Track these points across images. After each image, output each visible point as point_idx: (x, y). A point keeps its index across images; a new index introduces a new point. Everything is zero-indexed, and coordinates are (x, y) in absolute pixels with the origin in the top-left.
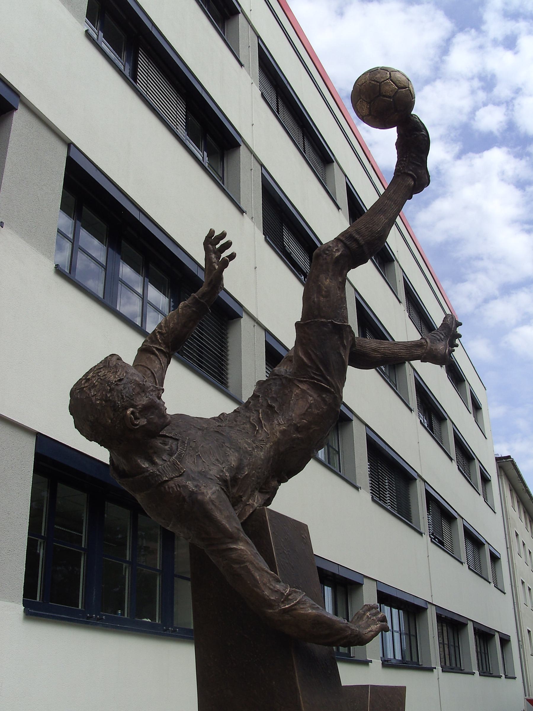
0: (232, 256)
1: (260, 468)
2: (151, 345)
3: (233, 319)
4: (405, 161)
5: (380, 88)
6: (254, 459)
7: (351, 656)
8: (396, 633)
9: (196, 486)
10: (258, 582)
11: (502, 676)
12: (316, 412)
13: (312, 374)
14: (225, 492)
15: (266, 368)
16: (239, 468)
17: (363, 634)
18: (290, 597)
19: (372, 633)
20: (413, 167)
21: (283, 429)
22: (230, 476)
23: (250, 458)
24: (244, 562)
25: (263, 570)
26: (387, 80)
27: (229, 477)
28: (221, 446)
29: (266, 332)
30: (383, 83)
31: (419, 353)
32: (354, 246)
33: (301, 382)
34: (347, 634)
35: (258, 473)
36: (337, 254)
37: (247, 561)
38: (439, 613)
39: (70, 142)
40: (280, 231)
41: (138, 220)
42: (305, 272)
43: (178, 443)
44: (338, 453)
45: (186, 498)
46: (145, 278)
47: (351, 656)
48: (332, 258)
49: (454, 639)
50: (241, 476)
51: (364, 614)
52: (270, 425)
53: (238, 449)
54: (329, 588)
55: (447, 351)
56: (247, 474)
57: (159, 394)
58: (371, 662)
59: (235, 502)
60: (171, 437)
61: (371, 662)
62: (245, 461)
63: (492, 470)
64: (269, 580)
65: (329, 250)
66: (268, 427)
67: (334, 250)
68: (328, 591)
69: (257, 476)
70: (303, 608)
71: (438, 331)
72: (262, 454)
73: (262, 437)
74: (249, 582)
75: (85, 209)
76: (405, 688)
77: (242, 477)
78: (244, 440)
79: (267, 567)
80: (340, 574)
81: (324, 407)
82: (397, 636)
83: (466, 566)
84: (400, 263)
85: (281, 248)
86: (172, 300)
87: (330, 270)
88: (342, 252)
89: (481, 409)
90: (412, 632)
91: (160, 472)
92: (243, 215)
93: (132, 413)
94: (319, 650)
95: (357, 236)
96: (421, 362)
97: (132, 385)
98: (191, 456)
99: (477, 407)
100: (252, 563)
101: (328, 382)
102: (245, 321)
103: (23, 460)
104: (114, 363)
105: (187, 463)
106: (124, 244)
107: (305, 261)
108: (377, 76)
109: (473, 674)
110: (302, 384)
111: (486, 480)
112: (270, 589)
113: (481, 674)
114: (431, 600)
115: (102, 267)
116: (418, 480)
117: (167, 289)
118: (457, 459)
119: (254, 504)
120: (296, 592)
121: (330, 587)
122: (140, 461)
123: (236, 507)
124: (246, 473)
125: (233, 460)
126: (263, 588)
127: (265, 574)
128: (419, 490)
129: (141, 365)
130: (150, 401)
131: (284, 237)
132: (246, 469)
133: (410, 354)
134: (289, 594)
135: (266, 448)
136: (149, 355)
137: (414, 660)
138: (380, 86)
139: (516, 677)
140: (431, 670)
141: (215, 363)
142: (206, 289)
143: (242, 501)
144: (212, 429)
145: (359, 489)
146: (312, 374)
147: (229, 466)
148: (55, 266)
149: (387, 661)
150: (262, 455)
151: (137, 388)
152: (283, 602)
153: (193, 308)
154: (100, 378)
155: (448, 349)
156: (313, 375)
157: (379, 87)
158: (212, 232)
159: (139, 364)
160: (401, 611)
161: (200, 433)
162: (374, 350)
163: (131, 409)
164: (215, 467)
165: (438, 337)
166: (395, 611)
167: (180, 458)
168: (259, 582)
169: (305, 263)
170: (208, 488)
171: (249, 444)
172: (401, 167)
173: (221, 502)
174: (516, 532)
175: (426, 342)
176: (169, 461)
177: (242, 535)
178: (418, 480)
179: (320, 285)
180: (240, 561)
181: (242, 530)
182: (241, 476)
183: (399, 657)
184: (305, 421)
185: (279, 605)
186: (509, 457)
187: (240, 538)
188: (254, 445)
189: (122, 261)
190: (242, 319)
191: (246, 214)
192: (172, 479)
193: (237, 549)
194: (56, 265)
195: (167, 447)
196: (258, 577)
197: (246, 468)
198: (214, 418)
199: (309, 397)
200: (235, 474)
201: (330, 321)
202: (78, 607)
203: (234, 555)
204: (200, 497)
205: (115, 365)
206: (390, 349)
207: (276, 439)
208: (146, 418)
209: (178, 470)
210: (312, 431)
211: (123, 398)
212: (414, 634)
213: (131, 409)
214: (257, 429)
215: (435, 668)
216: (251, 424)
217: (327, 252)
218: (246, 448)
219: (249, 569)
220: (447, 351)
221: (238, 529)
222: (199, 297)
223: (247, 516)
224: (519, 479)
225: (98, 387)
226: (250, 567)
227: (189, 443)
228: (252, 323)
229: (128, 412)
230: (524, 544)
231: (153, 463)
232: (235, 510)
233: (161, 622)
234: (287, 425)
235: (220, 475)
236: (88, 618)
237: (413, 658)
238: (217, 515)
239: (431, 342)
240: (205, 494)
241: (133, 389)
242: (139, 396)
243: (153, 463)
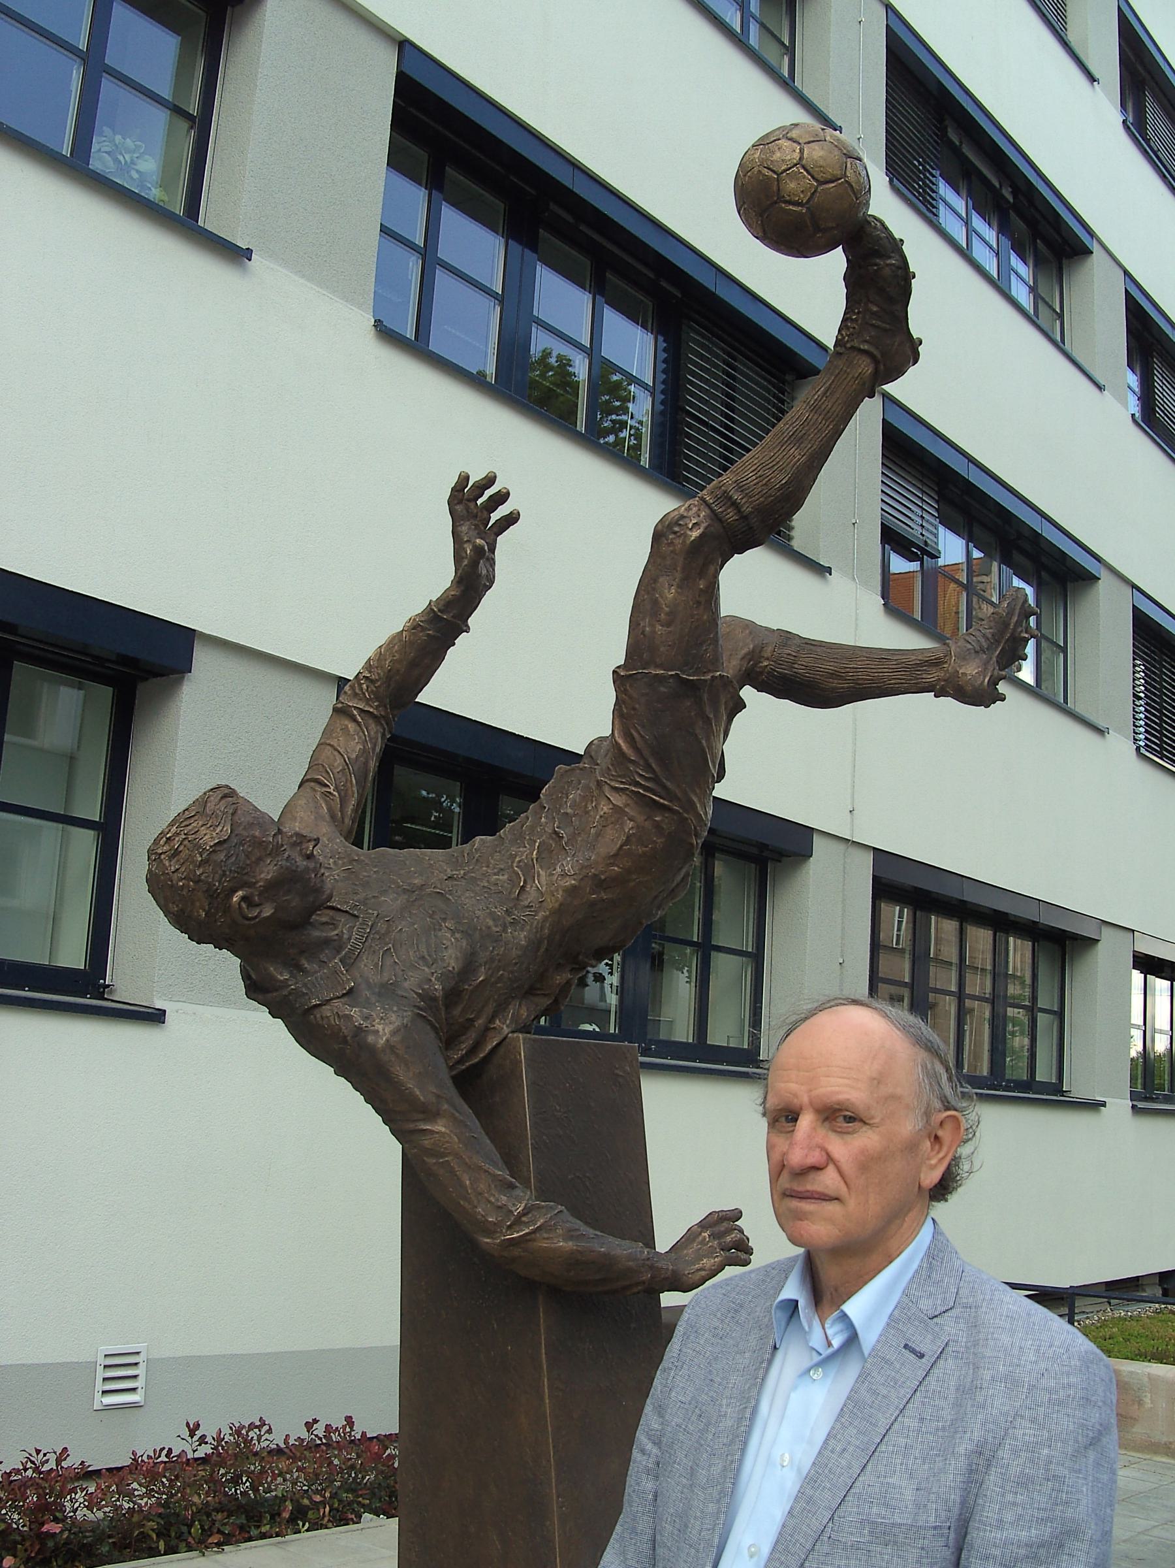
0: (511, 519)
1: (516, 964)
3: (805, 377)
4: (856, 320)
5: (778, 184)
6: (503, 949)
10: (467, 1191)
12: (641, 850)
13: (636, 777)
15: (882, 481)
17: (684, 1274)
19: (703, 1273)
20: (873, 333)
21: (571, 885)
23: (493, 948)
26: (793, 167)
27: (441, 993)
28: (437, 927)
29: (885, 398)
30: (785, 174)
31: (933, 679)
32: (731, 515)
34: (644, 1278)
35: (512, 972)
36: (695, 534)
37: (449, 1153)
39: (402, 39)
41: (569, 189)
44: (1064, 650)
45: (349, 1038)
48: (684, 541)
50: (470, 985)
52: (549, 876)
55: (986, 680)
56: (482, 981)
58: (1104, 1104)
61: (1104, 1104)
64: (489, 1186)
65: (680, 525)
69: (509, 978)
73: (529, 900)
74: (451, 1189)
75: (450, 171)
77: (471, 987)
78: (488, 911)
81: (659, 841)
87: (679, 569)
88: (706, 528)
96: (936, 696)
97: (246, 846)
98: (374, 951)
103: (310, 736)
105: (363, 966)
108: (775, 158)
110: (617, 795)
119: (502, 1028)
122: (275, 969)
124: (481, 979)
125: (452, 959)
129: (329, 745)
130: (282, 870)
132: (483, 970)
133: (911, 680)
135: (535, 922)
138: (778, 180)
142: (453, 593)
146: (636, 777)
147: (444, 970)
148: (373, 323)
150: (523, 939)
151: (256, 850)
153: (429, 630)
154: (187, 838)
156: (638, 780)
157: (776, 183)
158: (464, 479)
159: (328, 742)
168: (470, 1191)
171: (495, 918)
172: (847, 335)
179: (656, 599)
182: (470, 985)
184: (616, 868)
187: (441, 1112)
193: (433, 1131)
196: (468, 1182)
199: (628, 822)
200: (456, 983)
201: (672, 675)
206: (869, 670)
207: (557, 905)
214: (522, 884)
218: (489, 928)
222: (439, 610)
235: (423, 990)
240: (380, 1033)
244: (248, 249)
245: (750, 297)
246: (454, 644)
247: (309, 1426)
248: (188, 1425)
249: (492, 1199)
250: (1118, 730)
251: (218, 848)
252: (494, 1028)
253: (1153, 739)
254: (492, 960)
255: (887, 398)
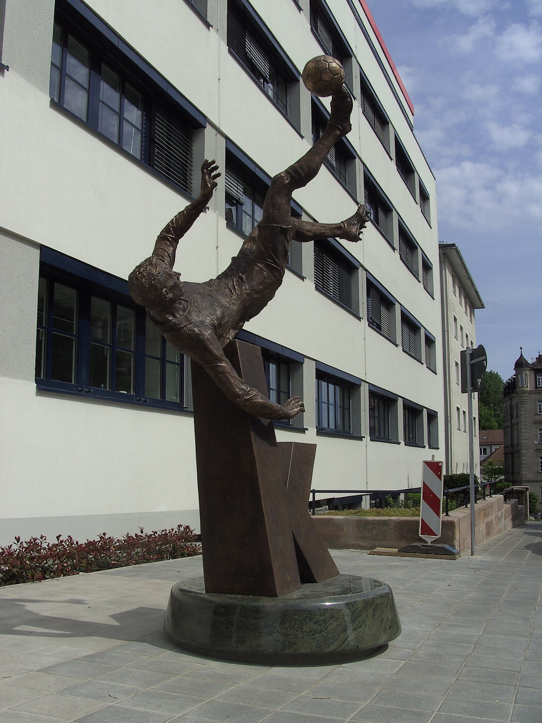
2: (167, 235)
7: (291, 424)
8: (331, 406)
9: (199, 331)
11: (426, 446)
12: (269, 281)
14: (214, 333)
16: (223, 317)
18: (250, 393)
22: (217, 323)
24: (224, 373)
25: (235, 377)
29: (227, 139)
33: (260, 263)
38: (372, 389)
40: (242, 35)
42: (265, 76)
43: (188, 304)
46: (122, 95)
47: (291, 424)
49: (384, 413)
51: (291, 402)
53: (221, 306)
54: (273, 365)
55: (357, 233)
57: (178, 277)
59: (220, 336)
60: (183, 300)
62: (226, 313)
63: (434, 258)
66: (239, 290)
67: (285, 179)
68: (273, 368)
70: (257, 399)
71: (352, 220)
72: (235, 307)
75: (71, 38)
76: (316, 445)
79: (236, 375)
80: (283, 354)
82: (332, 408)
83: (400, 348)
84: (357, 58)
85: (243, 54)
86: (144, 113)
89: (429, 199)
90: (346, 405)
91: (179, 322)
92: (209, 29)
93: (166, 291)
94: (266, 422)
95: (300, 170)
99: (424, 197)
100: (229, 374)
101: (276, 263)
102: (208, 131)
104: (155, 262)
106: (105, 68)
107: (265, 65)
109: (399, 443)
111: (427, 267)
112: (240, 388)
113: (406, 444)
114: (365, 378)
115: (85, 90)
116: (360, 268)
117: (140, 103)
118: (400, 248)
120: (253, 390)
121: (274, 364)
123: (220, 340)
126: (235, 387)
127: (237, 380)
128: (362, 276)
131: (246, 43)
134: (249, 391)
136: (165, 241)
137: (346, 430)
139: (439, 448)
140: (360, 438)
141: (180, 169)
143: (223, 336)
144: (206, 293)
145: (305, 279)
148: (50, 100)
149: (322, 430)
152: (246, 395)
155: (358, 232)
160: (338, 388)
161: (199, 296)
162: (308, 231)
163: (165, 289)
164: (209, 318)
165: (353, 222)
166: (331, 387)
167: (189, 313)
169: (265, 67)
170: (206, 332)
171: (228, 302)
173: (213, 340)
174: (454, 316)
175: (345, 226)
176: (184, 315)
177: (224, 358)
178: (360, 268)
180: (223, 372)
181: (224, 355)
183: (332, 426)
185: (244, 397)
186: (454, 245)
188: (231, 303)
189: (103, 81)
190: (206, 130)
191: (212, 28)
192: (186, 326)
194: (51, 99)
195: (181, 306)
197: (226, 318)
198: (205, 283)
202: (41, 377)
203: (220, 369)
204: (201, 337)
205: (155, 264)
207: (244, 299)
208: (172, 293)
209: (189, 321)
210: (265, 293)
211: (161, 284)
212: (348, 407)
213: (165, 289)
215: (364, 437)
216: (229, 288)
217: (280, 180)
218: (226, 305)
219: (228, 377)
220: (357, 233)
221: (222, 355)
223: (226, 345)
224: (462, 266)
225: (147, 277)
226: (228, 376)
227: (194, 303)
228: (215, 132)
229: (164, 291)
230: (461, 328)
231: (175, 317)
232: (219, 341)
233: (135, 394)
234: (250, 290)
236: (80, 391)
237: (346, 428)
238: (211, 346)
239: (347, 226)
241: (166, 277)
242: (169, 281)
243: (175, 317)
244: (7, 66)
245: (179, 95)
246: (199, 216)
247: (58, 537)
248: (16, 538)
249: (240, 387)
250: (309, 279)
251: (158, 275)
252: (227, 338)
253: (320, 283)
254: (228, 315)
255: (227, 138)
